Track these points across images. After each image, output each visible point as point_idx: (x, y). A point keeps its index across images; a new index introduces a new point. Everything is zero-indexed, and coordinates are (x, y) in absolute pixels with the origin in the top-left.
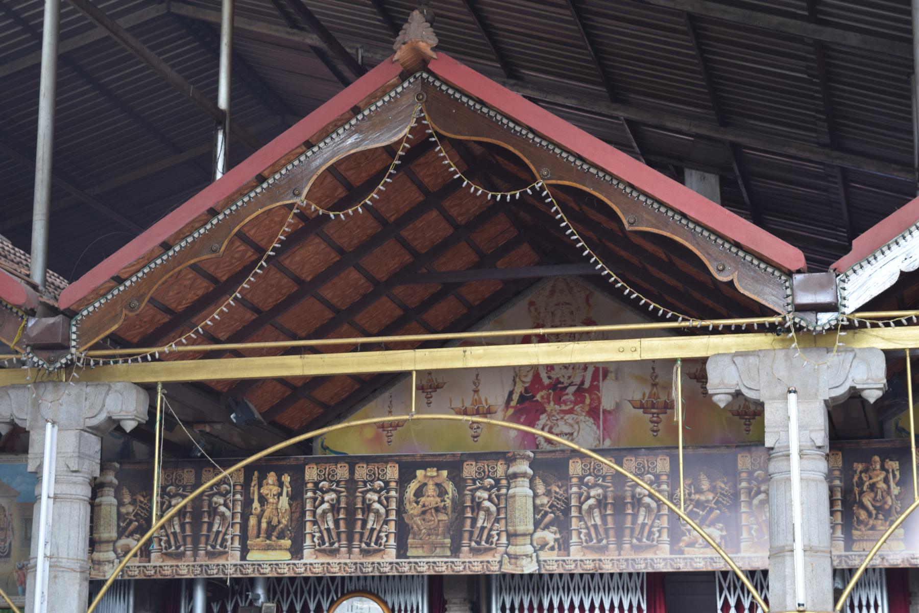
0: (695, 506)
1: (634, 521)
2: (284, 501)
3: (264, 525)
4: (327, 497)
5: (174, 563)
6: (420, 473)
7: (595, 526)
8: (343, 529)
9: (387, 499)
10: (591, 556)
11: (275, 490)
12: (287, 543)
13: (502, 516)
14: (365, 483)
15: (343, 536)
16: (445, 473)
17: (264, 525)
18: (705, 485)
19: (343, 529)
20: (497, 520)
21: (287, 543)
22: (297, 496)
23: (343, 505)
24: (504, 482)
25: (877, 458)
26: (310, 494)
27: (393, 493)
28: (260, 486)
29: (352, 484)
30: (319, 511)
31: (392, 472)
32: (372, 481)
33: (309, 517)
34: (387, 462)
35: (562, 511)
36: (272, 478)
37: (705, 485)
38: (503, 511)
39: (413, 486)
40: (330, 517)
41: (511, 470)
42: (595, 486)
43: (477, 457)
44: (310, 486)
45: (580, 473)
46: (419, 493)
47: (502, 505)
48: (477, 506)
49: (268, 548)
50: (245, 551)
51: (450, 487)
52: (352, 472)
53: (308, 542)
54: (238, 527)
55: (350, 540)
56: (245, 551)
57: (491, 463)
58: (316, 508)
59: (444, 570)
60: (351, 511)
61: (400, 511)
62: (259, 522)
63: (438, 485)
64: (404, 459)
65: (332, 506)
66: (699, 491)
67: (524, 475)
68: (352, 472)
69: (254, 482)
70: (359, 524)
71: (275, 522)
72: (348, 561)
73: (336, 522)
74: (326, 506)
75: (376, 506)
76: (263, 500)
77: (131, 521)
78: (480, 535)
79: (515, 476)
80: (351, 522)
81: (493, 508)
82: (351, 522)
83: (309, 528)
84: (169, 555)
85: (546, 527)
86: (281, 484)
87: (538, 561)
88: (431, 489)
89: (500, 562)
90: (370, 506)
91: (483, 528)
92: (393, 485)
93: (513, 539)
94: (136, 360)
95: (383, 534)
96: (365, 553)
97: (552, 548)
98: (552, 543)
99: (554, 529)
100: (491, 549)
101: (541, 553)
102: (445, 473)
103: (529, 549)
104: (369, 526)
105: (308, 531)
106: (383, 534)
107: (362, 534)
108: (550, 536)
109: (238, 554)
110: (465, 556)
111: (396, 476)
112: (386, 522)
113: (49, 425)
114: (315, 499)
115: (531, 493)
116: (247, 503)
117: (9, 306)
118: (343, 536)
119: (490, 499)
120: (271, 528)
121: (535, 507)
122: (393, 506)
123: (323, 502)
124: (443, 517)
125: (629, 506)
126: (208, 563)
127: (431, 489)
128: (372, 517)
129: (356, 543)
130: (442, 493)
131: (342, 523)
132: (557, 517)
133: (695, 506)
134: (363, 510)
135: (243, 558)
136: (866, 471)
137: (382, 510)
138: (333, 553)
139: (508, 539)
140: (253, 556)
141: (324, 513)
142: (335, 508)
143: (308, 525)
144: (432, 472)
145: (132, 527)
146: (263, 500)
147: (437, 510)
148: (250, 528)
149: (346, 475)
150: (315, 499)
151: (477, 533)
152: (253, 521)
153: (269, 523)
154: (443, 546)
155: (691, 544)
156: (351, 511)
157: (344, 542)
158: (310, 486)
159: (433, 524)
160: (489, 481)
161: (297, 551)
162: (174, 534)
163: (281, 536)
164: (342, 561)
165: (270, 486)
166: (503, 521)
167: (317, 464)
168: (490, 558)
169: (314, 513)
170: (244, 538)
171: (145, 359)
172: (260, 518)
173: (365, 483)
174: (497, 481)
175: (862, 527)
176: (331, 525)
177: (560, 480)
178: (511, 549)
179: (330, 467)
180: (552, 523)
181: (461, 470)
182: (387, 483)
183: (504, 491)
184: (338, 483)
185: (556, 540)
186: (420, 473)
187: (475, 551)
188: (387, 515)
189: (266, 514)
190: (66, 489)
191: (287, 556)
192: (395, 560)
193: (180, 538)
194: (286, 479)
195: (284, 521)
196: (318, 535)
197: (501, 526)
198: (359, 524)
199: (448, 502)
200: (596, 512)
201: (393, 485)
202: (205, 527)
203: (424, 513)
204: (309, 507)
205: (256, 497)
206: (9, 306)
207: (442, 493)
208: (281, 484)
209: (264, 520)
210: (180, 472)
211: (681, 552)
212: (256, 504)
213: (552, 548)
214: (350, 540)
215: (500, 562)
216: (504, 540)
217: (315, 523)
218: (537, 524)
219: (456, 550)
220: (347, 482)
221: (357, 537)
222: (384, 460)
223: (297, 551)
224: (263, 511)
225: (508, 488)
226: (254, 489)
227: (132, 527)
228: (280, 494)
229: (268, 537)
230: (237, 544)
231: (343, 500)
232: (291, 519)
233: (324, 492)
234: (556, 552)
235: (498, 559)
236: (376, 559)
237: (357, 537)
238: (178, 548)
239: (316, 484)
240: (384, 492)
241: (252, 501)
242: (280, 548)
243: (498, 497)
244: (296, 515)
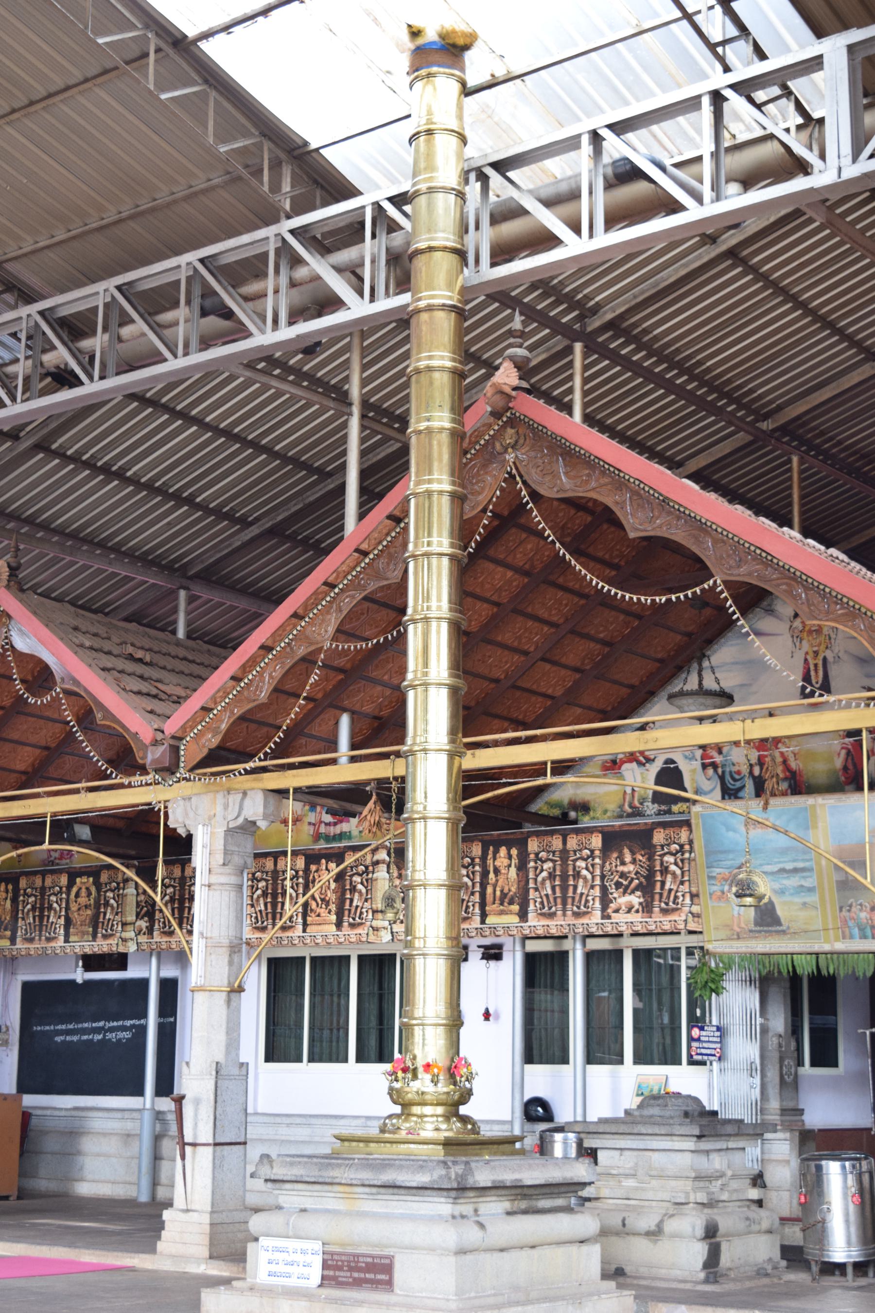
0: (621, 877)
1: (662, 887)
2: (513, 871)
3: (498, 893)
4: (546, 866)
5: (168, 939)
6: (78, 880)
7: (547, 896)
11: (506, 862)
12: (8, 933)
13: (686, 878)
14: (662, 846)
15: (559, 901)
16: (91, 879)
17: (498, 893)
18: (628, 858)
20: (682, 883)
21: (516, 908)
22: (522, 867)
23: (558, 873)
24: (371, 868)
25: (323, 861)
26: (532, 864)
27: (597, 861)
28: (495, 859)
31: (64, 880)
32: (668, 845)
34: (592, 833)
35: (644, 877)
36: (503, 851)
37: (628, 858)
38: (687, 873)
39: (74, 890)
40: (548, 884)
43: (664, 825)
44: (532, 856)
46: (77, 895)
47: (686, 869)
49: (502, 913)
50: (484, 916)
51: (93, 889)
52: (565, 842)
54: (477, 895)
55: (564, 904)
56: (484, 916)
57: (676, 830)
58: (537, 876)
59: (88, 951)
60: (564, 877)
61: (67, 908)
62: (495, 891)
63: (87, 889)
65: (550, 873)
66: (623, 863)
67: (383, 862)
68: (565, 842)
69: (490, 856)
70: (571, 889)
71: (506, 891)
72: (563, 923)
73: (553, 888)
78: (355, 913)
79: (377, 863)
80: (564, 888)
82: (564, 888)
83: (532, 894)
84: (164, 933)
87: (392, 933)
88: (83, 893)
89: (686, 921)
91: (670, 890)
93: (696, 900)
97: (637, 911)
98: (637, 907)
99: (638, 893)
100: (677, 909)
101: (394, 926)
102: (91, 879)
104: (667, 887)
105: (531, 897)
106: (679, 894)
107: (661, 895)
111: (600, 845)
112: (592, 887)
113: (200, 827)
114: (536, 868)
116: (485, 874)
118: (559, 901)
120: (504, 895)
121: (137, 903)
122: (64, 905)
123: (542, 870)
124: (89, 912)
125: (658, 873)
126: (575, 922)
127: (83, 893)
128: (669, 878)
129: (569, 906)
131: (558, 889)
132: (641, 883)
133: (621, 877)
134: (661, 871)
135: (483, 922)
136: (317, 871)
137: (589, 876)
138: (552, 916)
139: (692, 900)
140: (491, 920)
142: (552, 876)
143: (531, 891)
144: (84, 879)
145: (633, 885)
146: (497, 871)
148: (488, 896)
149: (272, 867)
150: (536, 868)
151: (665, 894)
152: (489, 890)
153: (502, 891)
155: (617, 911)
156: (564, 877)
157: (559, 906)
158: (532, 856)
159: (83, 918)
160: (586, 852)
161: (523, 915)
163: (511, 903)
164: (559, 923)
165: (502, 859)
166: (687, 884)
167: (537, 836)
168: (677, 918)
170: (483, 904)
173: (662, 846)
175: (313, 915)
176: (549, 892)
177: (643, 849)
180: (636, 889)
183: (687, 855)
184: (554, 852)
185: (641, 904)
186: (78, 880)
187: (665, 912)
188: (593, 881)
189: (500, 883)
190: (214, 879)
191: (516, 919)
195: (513, 889)
196: (539, 900)
198: (571, 889)
199: (92, 901)
200: (31, 915)
201: (597, 853)
203: (79, 909)
204: (20, 908)
207: (89, 894)
208: (510, 857)
209: (498, 889)
210: (550, 839)
211: (609, 917)
212: (492, 875)
213: (637, 911)
214: (564, 904)
215: (686, 921)
216: (688, 900)
217: (536, 889)
221: (570, 901)
222: (60, 872)
223: (523, 915)
224: (497, 881)
225: (373, 873)
226: (490, 862)
227: (633, 885)
228: (510, 866)
229: (502, 904)
231: (558, 868)
232: (518, 888)
233: (543, 862)
234: (640, 914)
235: (684, 918)
236: (585, 920)
240: (679, 855)
241: (489, 872)
242: (511, 913)
243: (682, 861)
244: (523, 883)
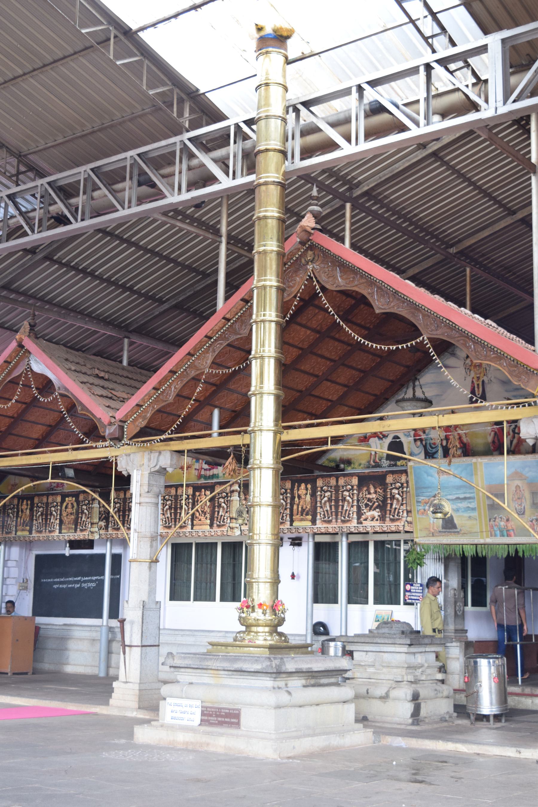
2: (308, 497)
3: (300, 509)
4: (327, 494)
6: (67, 499)
8: (333, 510)
9: (353, 494)
10: (326, 525)
11: (304, 492)
12: (28, 528)
13: (404, 502)
15: (334, 514)
16: (74, 499)
17: (300, 509)
18: (372, 490)
19: (333, 510)
20: (402, 505)
21: (310, 517)
22: (313, 495)
23: (333, 498)
24: (405, 485)
25: (203, 490)
26: (319, 493)
28: (298, 490)
29: (337, 488)
30: (323, 501)
31: (59, 499)
33: (318, 505)
34: (352, 476)
36: (303, 486)
37: (372, 490)
39: (65, 504)
40: (328, 504)
41: (232, 489)
42: (327, 491)
43: (393, 472)
44: (319, 489)
45: (321, 485)
46: (66, 507)
47: (404, 497)
48: (393, 497)
49: (302, 520)
52: (337, 481)
53: (318, 517)
54: (288, 510)
55: (337, 515)
56: (292, 521)
57: (399, 475)
59: (72, 538)
60: (337, 501)
62: (298, 508)
63: (72, 504)
64: (360, 474)
65: (329, 498)
66: (370, 493)
67: (236, 491)
68: (337, 481)
69: (296, 488)
71: (304, 508)
73: (331, 507)
74: (326, 499)
75: (397, 496)
76: (299, 497)
77: (375, 502)
78: (394, 512)
79: (233, 491)
81: (400, 498)
82: (337, 507)
83: (319, 510)
84: (325, 521)
85: (375, 509)
86: (307, 489)
89: (404, 526)
90: (394, 496)
91: (346, 510)
92: (289, 491)
93: (409, 514)
94: (524, 406)
95: (401, 511)
96: (343, 522)
97: (377, 520)
98: (377, 517)
99: (378, 510)
100: (399, 519)
102: (74, 499)
103: (97, 529)
106: (401, 511)
108: (103, 524)
109: (289, 523)
110: (79, 533)
111: (357, 483)
112: (352, 506)
113: (135, 471)
114: (321, 495)
115: (238, 499)
116: (293, 498)
117: (532, 370)
118: (334, 514)
119: (399, 494)
120: (303, 510)
123: (324, 497)
128: (346, 503)
129: (339, 517)
130: (73, 507)
131: (333, 507)
134: (342, 500)
135: (291, 525)
136: (199, 496)
137: (351, 500)
138: (329, 522)
139: (407, 514)
140: (295, 524)
141: (325, 502)
142: (330, 500)
143: (318, 508)
144: (70, 499)
145: (375, 506)
146: (299, 497)
147: (71, 514)
149: (335, 483)
150: (321, 495)
152: (295, 507)
153: (302, 508)
154: (72, 528)
155: (366, 520)
156: (337, 501)
157: (334, 517)
158: (319, 489)
162: (327, 511)
163: (26, 526)
168: (399, 524)
169: (321, 502)
170: (291, 515)
171: (530, 405)
172: (298, 505)
174: (402, 484)
176: (328, 508)
178: (231, 525)
179: (328, 479)
181: (385, 479)
182: (352, 487)
183: (405, 489)
184: (331, 487)
185: (379, 516)
186: (67, 499)
187: (392, 520)
188: (286, 505)
189: (301, 504)
192: (356, 525)
193: (329, 513)
194: (309, 486)
195: (308, 507)
197: (404, 507)
201: (289, 491)
202: (389, 505)
204: (318, 499)
205: (296, 496)
206: (532, 370)
207: (73, 507)
208: (307, 489)
209: (300, 507)
211: (361, 523)
212: (296, 499)
214: (337, 515)
215: (404, 526)
216: (405, 514)
217: (321, 507)
218: (100, 518)
219: (76, 531)
220: (335, 486)
221: (340, 514)
222: (57, 494)
226: (296, 492)
227: (375, 506)
228: (306, 494)
229: (302, 515)
230: (288, 518)
231: (333, 495)
233: (325, 492)
235: (403, 524)
237: (340, 514)
238: (329, 518)
239: (322, 488)
242: (307, 520)
243: (402, 492)
244: (314, 504)
